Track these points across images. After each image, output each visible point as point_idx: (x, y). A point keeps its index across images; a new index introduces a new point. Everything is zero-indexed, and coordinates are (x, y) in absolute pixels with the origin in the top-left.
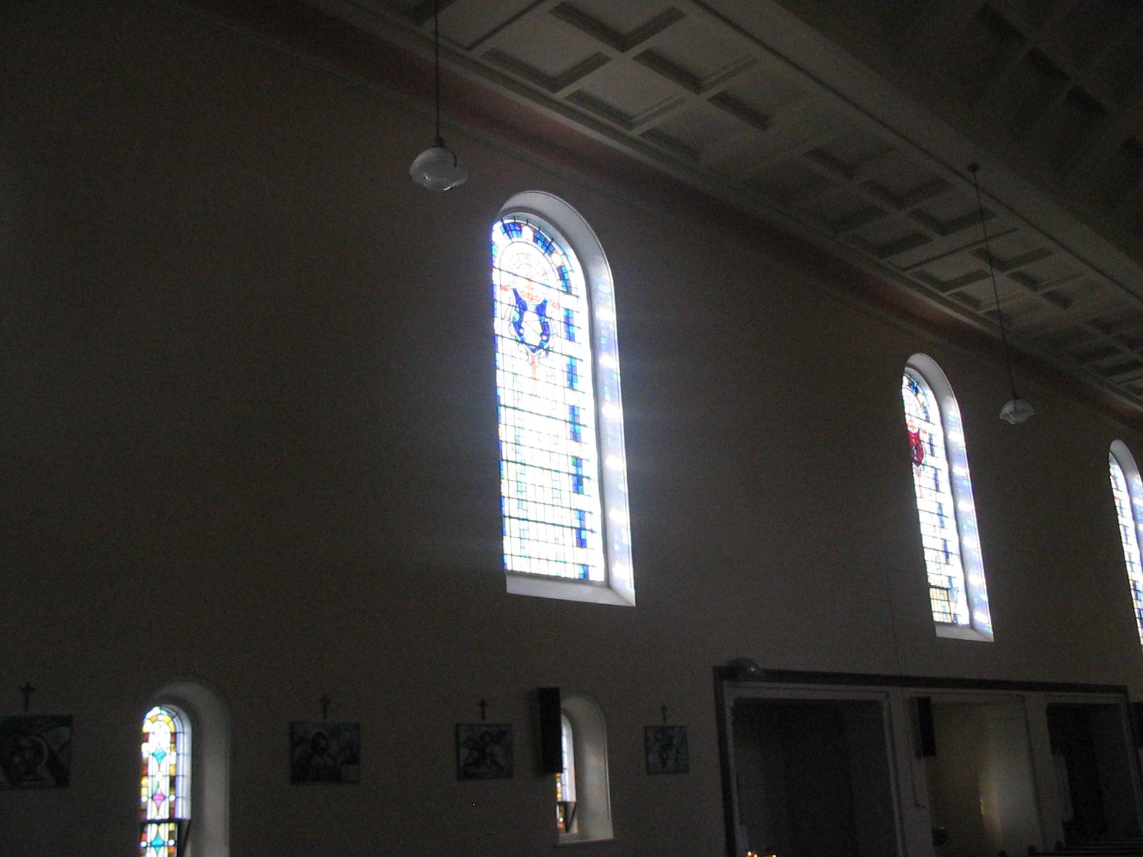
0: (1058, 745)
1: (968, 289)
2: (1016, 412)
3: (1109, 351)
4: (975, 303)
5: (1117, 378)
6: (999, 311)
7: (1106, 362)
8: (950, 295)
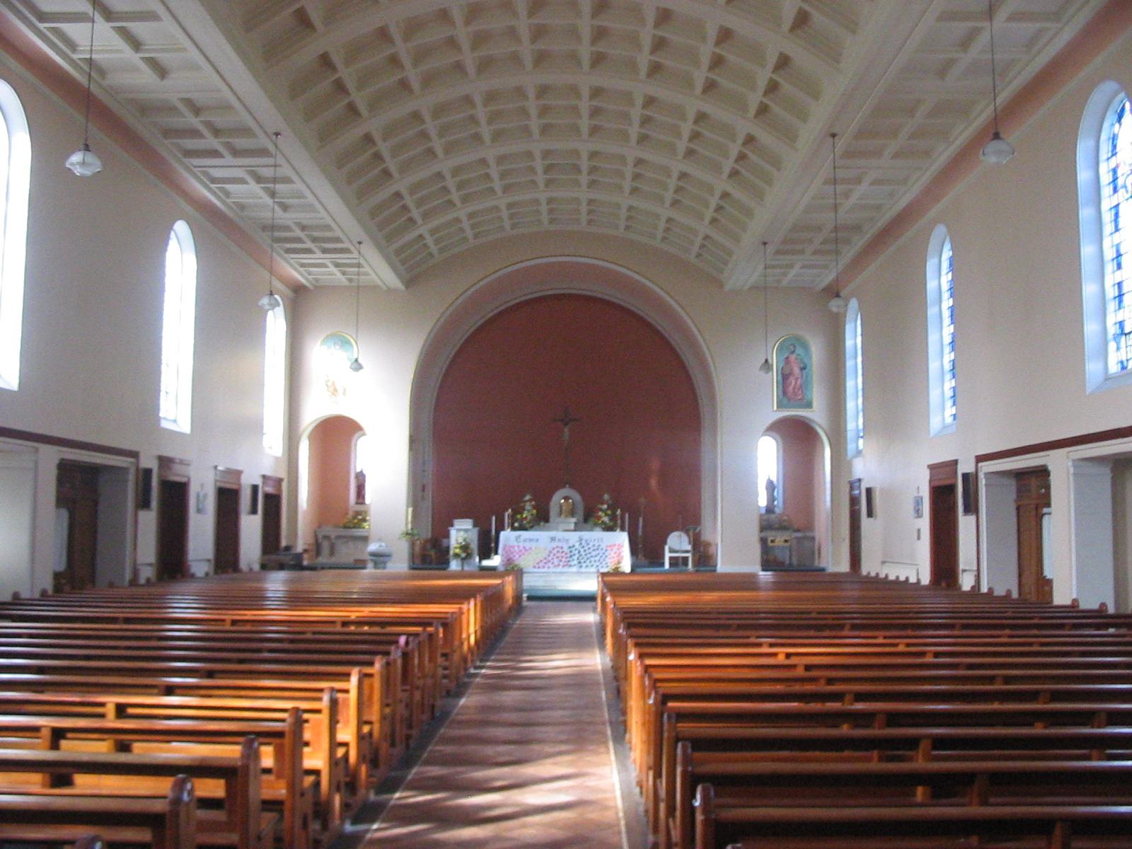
0: (62, 500)
1: (67, 28)
2: (83, 164)
3: (195, 133)
4: (72, 46)
5: (196, 162)
6: (91, 59)
7: (190, 144)
8: (48, 29)
